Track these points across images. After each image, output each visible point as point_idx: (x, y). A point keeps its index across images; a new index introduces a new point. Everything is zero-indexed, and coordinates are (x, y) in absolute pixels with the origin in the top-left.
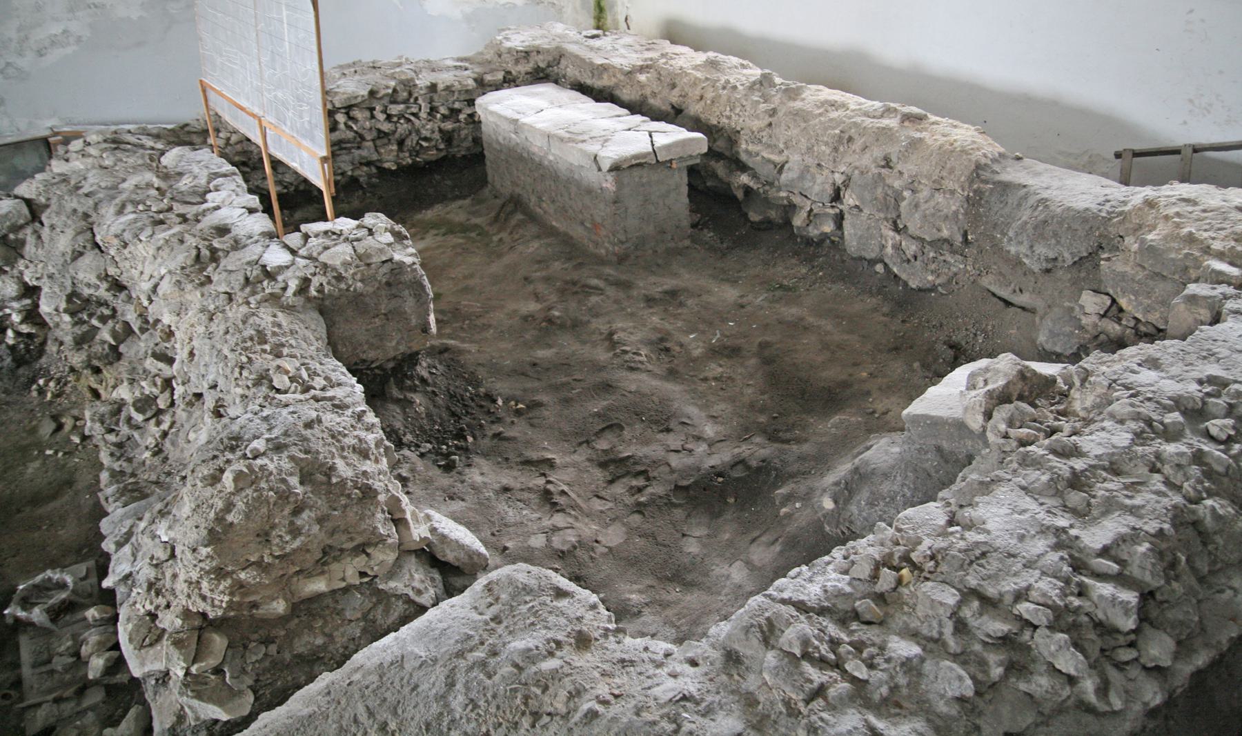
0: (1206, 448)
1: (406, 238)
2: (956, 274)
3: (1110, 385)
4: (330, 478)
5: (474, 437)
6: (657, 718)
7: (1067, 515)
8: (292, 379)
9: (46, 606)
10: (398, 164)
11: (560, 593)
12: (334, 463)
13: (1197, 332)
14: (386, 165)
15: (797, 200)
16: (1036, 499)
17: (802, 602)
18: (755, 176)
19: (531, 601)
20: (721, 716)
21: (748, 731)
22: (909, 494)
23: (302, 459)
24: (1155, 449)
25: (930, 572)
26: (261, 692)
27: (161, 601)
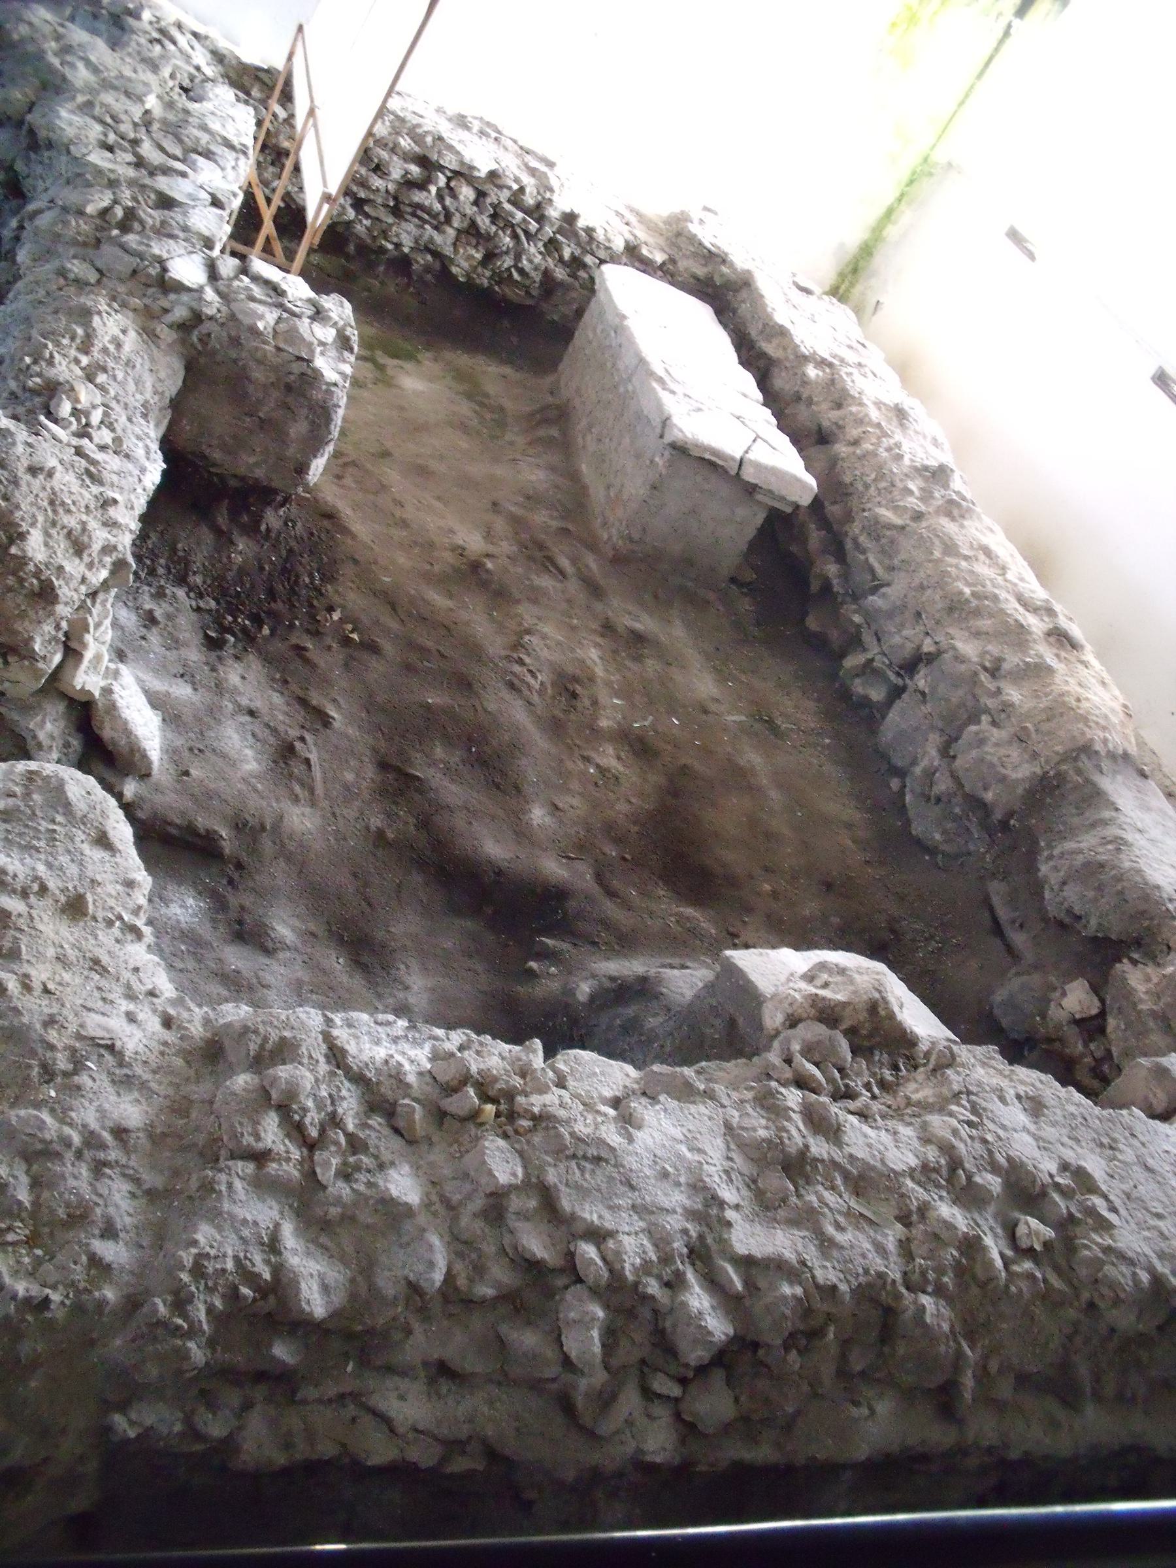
0: (988, 1241)
1: (351, 350)
2: (969, 854)
3: (960, 1092)
5: (273, 632)
6: (60, 1045)
7: (745, 1192)
8: (75, 412)
10: (468, 275)
11: (103, 841)
12: (28, 532)
13: (1124, 1112)
14: (454, 270)
15: (868, 638)
16: (729, 1149)
17: (343, 1052)
18: (845, 576)
19: (59, 823)
20: (131, 1098)
21: (141, 1135)
22: (668, 1049)
24: (927, 1198)
25: (517, 1132)
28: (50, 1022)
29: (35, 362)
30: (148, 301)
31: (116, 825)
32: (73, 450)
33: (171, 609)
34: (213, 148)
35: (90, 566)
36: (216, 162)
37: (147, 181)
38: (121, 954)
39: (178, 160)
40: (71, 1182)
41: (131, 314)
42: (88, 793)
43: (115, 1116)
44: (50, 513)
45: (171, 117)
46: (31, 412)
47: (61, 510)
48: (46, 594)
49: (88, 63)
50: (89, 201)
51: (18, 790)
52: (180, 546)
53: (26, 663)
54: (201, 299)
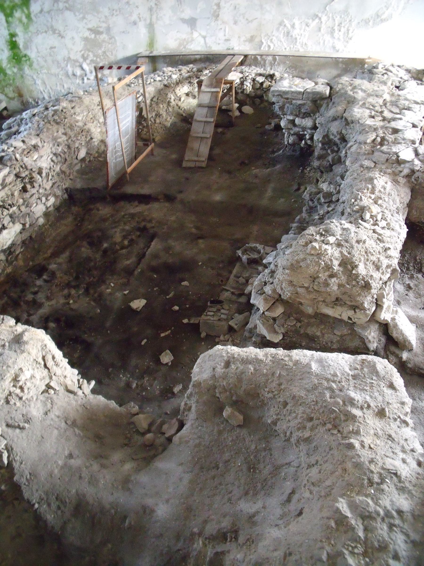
4: (353, 270)
6: (375, 471)
8: (372, 217)
9: (249, 257)
11: (391, 386)
12: (359, 264)
20: (404, 497)
23: (345, 255)
26: (286, 338)
27: (271, 280)
28: (371, 461)
29: (356, 201)
30: (393, 169)
31: (396, 379)
32: (372, 231)
33: (416, 283)
34: (410, 106)
35: (383, 273)
36: (412, 110)
37: (388, 125)
38: (400, 433)
39: (398, 114)
40: (380, 531)
41: (388, 176)
42: (385, 367)
43: (398, 504)
44: (366, 256)
45: (393, 99)
46: (356, 219)
47: (369, 255)
48: (367, 286)
49: (362, 90)
50: (368, 138)
51: (358, 367)
52: (418, 258)
53: (362, 312)
54: (413, 164)
